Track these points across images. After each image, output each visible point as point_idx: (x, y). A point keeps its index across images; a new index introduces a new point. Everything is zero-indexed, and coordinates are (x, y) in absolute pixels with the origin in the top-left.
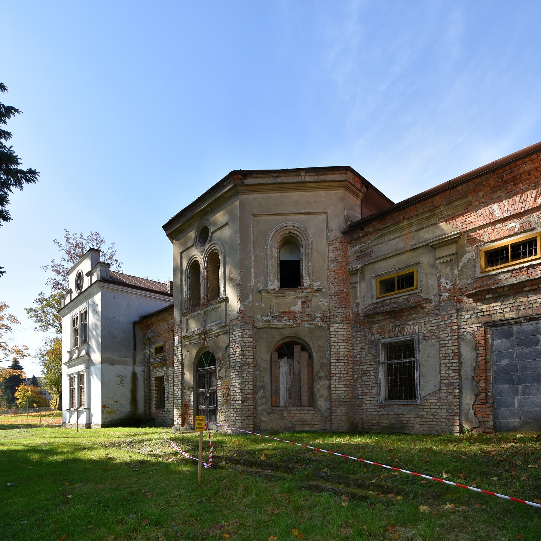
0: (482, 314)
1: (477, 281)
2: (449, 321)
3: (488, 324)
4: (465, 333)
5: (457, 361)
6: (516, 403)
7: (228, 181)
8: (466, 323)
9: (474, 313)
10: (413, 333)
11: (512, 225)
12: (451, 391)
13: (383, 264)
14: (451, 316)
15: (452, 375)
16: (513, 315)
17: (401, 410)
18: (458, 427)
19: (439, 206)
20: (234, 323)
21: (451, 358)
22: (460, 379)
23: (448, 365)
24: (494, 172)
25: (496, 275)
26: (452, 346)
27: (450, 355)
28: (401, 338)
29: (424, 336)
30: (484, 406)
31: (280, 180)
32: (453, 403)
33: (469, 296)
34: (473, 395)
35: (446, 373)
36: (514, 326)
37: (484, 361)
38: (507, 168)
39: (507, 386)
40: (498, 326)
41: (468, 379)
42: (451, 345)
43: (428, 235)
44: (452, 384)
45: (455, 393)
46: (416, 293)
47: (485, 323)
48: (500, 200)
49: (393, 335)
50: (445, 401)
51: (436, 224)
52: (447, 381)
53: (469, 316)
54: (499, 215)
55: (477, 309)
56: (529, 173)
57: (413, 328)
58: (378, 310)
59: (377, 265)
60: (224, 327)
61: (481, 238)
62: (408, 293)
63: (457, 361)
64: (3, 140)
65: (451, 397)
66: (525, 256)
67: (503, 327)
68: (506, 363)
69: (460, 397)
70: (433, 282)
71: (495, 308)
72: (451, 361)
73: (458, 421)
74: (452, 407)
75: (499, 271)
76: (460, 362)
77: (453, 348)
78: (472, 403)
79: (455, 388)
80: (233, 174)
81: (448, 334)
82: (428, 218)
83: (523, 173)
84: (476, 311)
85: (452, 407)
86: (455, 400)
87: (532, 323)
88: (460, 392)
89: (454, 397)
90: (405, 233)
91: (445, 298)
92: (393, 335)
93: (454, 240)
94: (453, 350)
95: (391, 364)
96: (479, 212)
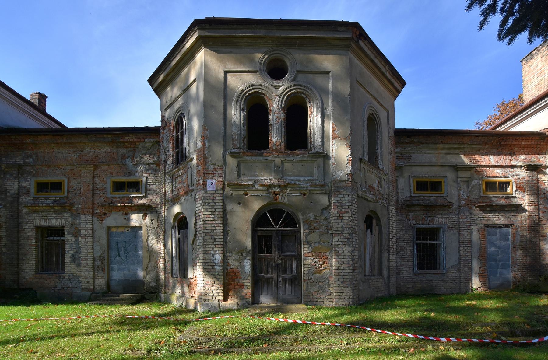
7: (344, 29)
10: (441, 223)
11: (498, 171)
13: (419, 169)
17: (429, 277)
20: (341, 185)
28: (432, 226)
29: (448, 227)
31: (377, 61)
43: (452, 159)
44: (467, 260)
46: (443, 197)
48: (494, 155)
49: (425, 223)
51: (458, 154)
52: (464, 258)
54: (493, 163)
57: (441, 220)
58: (414, 202)
59: (414, 169)
60: (322, 186)
62: (438, 195)
70: (455, 192)
80: (356, 26)
82: (455, 148)
90: (437, 152)
92: (425, 223)
93: (468, 168)
95: (420, 244)
96: (483, 157)
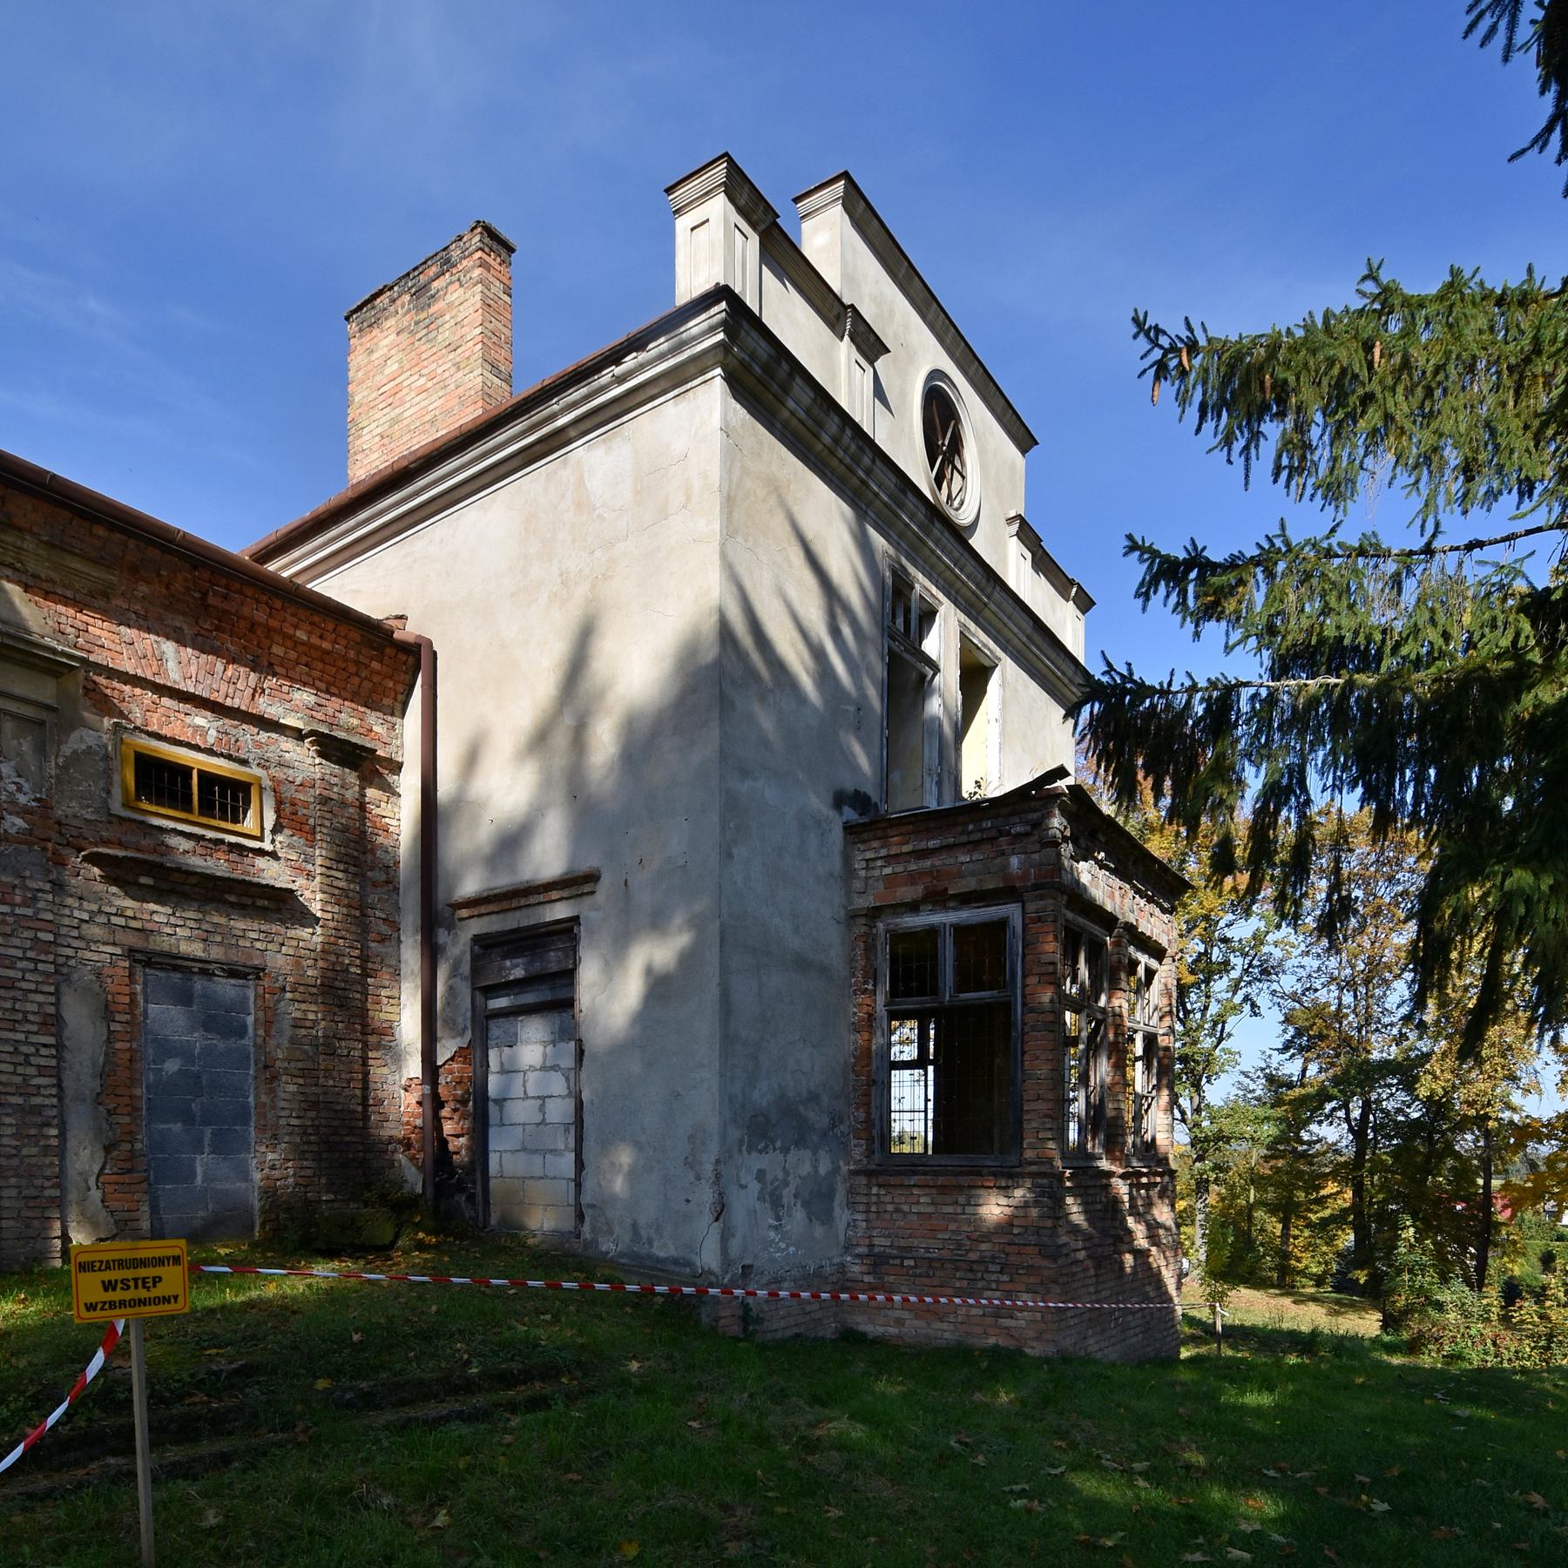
0: (121, 921)
1: (110, 822)
2: (29, 912)
3: (139, 956)
4: (72, 962)
5: (51, 1040)
6: (199, 1170)
8: (75, 933)
9: (100, 911)
12: (33, 1132)
14: (35, 899)
15: (36, 1081)
16: (196, 949)
18: (58, 1242)
19: (20, 530)
21: (34, 1028)
22: (60, 1097)
23: (25, 1049)
24: (195, 568)
25: (160, 829)
26: (36, 991)
27: (31, 1017)
30: (126, 1178)
32: (39, 1167)
33: (94, 859)
34: (99, 1146)
35: (14, 1073)
36: (196, 978)
37: (127, 1056)
38: (224, 581)
39: (177, 1127)
40: (161, 967)
41: (84, 1100)
42: (33, 987)
44: (37, 1110)
45: (48, 1137)
47: (131, 950)
50: (15, 1162)
53: (86, 917)
54: (173, 675)
55: (110, 904)
56: (253, 626)
61: (123, 706)
63: (51, 1040)
64: (1565, 1069)
65: (34, 1151)
66: (224, 818)
67: (172, 974)
68: (176, 1068)
69: (61, 1151)
71: (156, 918)
72: (34, 1039)
73: (58, 1225)
74: (38, 1182)
75: (171, 825)
76: (60, 1046)
77: (40, 998)
78: (96, 1169)
79: (48, 1125)
81: (25, 950)
83: (245, 618)
84: (108, 909)
85: (38, 1182)
86: (48, 1160)
87: (233, 981)
88: (62, 1136)
89: (46, 1150)
91: (13, 831)
94: (40, 1004)
